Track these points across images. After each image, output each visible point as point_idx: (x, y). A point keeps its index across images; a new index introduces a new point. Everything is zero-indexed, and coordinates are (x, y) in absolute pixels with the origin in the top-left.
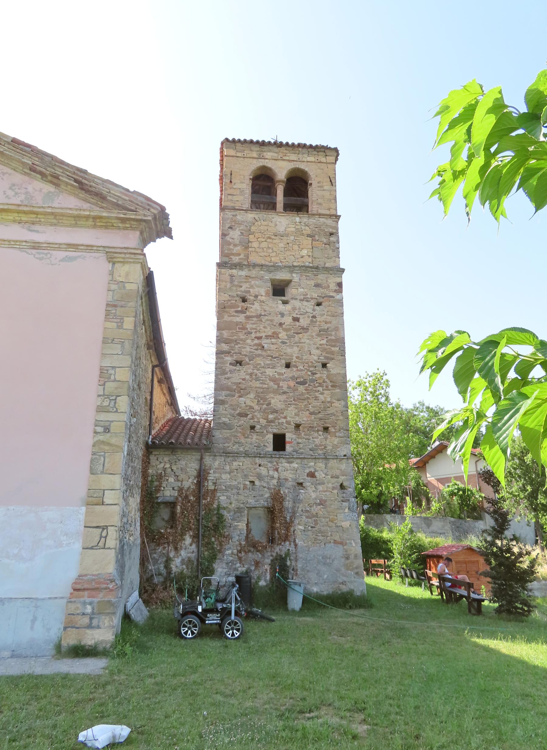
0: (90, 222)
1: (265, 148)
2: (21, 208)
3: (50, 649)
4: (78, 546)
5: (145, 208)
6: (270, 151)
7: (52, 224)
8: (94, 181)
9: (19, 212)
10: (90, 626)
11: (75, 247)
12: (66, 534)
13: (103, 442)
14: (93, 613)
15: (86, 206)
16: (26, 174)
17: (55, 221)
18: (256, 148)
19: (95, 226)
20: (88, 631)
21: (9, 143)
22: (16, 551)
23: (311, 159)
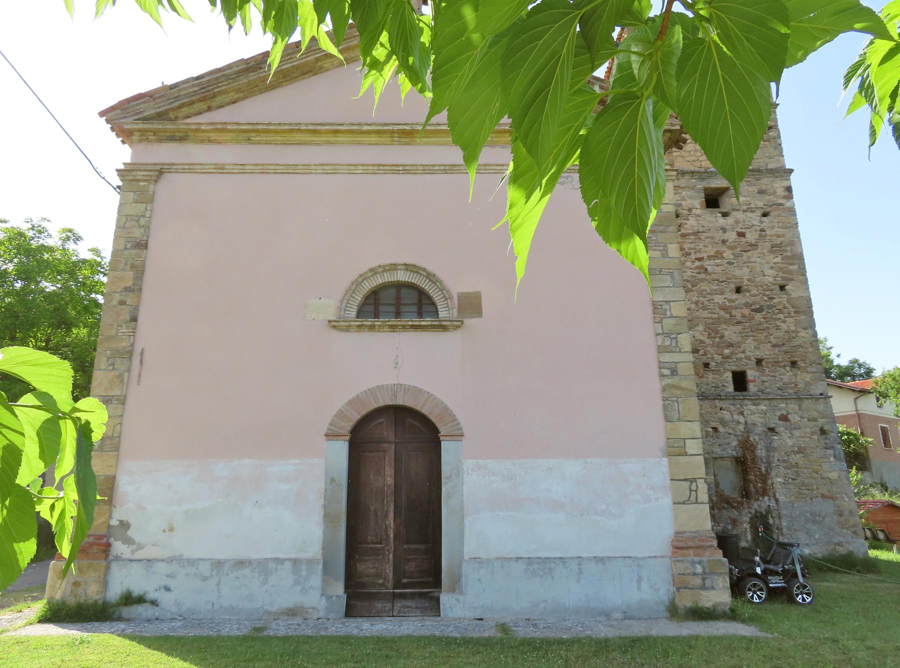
10: (703, 587)
14: (704, 573)
20: (702, 592)
22: (604, 507)
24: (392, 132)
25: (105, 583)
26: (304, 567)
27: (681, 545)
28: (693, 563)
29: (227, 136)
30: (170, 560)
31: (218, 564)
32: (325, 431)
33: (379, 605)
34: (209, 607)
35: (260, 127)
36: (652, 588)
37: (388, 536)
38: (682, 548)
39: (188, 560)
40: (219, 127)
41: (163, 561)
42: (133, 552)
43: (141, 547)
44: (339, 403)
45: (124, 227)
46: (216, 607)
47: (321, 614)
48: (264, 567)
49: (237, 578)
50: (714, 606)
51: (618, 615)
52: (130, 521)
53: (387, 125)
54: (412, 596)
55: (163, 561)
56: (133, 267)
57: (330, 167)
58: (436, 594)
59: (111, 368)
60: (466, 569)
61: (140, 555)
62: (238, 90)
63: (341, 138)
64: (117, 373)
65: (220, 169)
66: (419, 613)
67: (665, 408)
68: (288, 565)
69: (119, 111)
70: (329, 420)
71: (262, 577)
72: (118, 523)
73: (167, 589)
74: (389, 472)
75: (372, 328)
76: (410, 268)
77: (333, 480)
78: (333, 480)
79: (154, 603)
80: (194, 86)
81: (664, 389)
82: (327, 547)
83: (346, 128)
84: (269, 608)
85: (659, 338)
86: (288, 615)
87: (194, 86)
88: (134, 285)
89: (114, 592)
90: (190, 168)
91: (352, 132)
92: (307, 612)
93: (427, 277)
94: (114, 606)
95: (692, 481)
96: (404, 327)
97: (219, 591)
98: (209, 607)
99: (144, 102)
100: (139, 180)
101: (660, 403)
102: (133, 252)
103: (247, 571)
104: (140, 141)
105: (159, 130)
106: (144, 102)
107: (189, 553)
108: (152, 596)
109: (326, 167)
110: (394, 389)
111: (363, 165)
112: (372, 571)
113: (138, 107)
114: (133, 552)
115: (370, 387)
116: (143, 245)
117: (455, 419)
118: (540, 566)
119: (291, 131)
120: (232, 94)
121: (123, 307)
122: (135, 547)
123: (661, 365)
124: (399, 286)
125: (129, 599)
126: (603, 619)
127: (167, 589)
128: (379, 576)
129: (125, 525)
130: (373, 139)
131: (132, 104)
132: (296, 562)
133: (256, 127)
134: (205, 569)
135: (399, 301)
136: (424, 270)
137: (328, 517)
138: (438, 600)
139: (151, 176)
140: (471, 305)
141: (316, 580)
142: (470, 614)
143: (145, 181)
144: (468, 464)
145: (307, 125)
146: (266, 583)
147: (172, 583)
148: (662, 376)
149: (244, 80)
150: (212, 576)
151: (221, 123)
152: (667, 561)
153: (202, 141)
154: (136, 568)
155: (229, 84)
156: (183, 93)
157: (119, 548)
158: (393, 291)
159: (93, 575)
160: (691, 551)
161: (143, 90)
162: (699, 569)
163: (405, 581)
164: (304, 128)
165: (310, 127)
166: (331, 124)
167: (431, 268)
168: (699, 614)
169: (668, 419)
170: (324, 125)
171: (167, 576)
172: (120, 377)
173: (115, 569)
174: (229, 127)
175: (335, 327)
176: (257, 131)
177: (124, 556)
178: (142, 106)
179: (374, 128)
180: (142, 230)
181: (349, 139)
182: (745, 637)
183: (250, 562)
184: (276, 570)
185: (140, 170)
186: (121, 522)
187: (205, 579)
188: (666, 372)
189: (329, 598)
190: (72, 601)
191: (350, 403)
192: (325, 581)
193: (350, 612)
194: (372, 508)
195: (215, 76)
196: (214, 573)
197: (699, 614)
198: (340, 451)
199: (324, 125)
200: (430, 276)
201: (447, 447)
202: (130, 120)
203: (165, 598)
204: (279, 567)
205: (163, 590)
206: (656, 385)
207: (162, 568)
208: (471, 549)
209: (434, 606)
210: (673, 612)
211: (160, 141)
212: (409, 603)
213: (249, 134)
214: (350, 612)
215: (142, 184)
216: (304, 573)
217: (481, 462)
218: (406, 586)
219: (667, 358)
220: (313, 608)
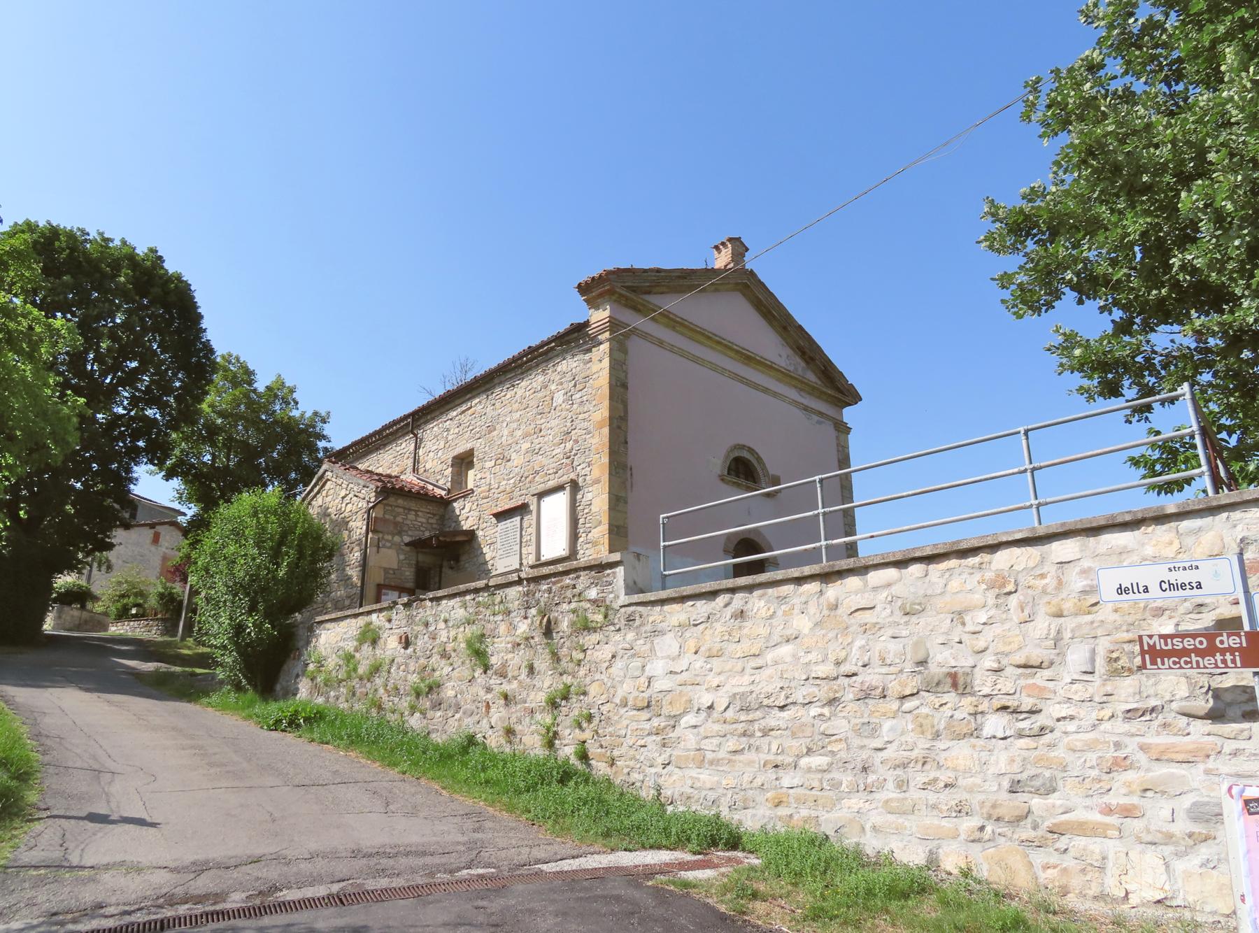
63: (730, 353)
91: (726, 346)
130: (732, 354)
135: (743, 470)
200: (759, 459)
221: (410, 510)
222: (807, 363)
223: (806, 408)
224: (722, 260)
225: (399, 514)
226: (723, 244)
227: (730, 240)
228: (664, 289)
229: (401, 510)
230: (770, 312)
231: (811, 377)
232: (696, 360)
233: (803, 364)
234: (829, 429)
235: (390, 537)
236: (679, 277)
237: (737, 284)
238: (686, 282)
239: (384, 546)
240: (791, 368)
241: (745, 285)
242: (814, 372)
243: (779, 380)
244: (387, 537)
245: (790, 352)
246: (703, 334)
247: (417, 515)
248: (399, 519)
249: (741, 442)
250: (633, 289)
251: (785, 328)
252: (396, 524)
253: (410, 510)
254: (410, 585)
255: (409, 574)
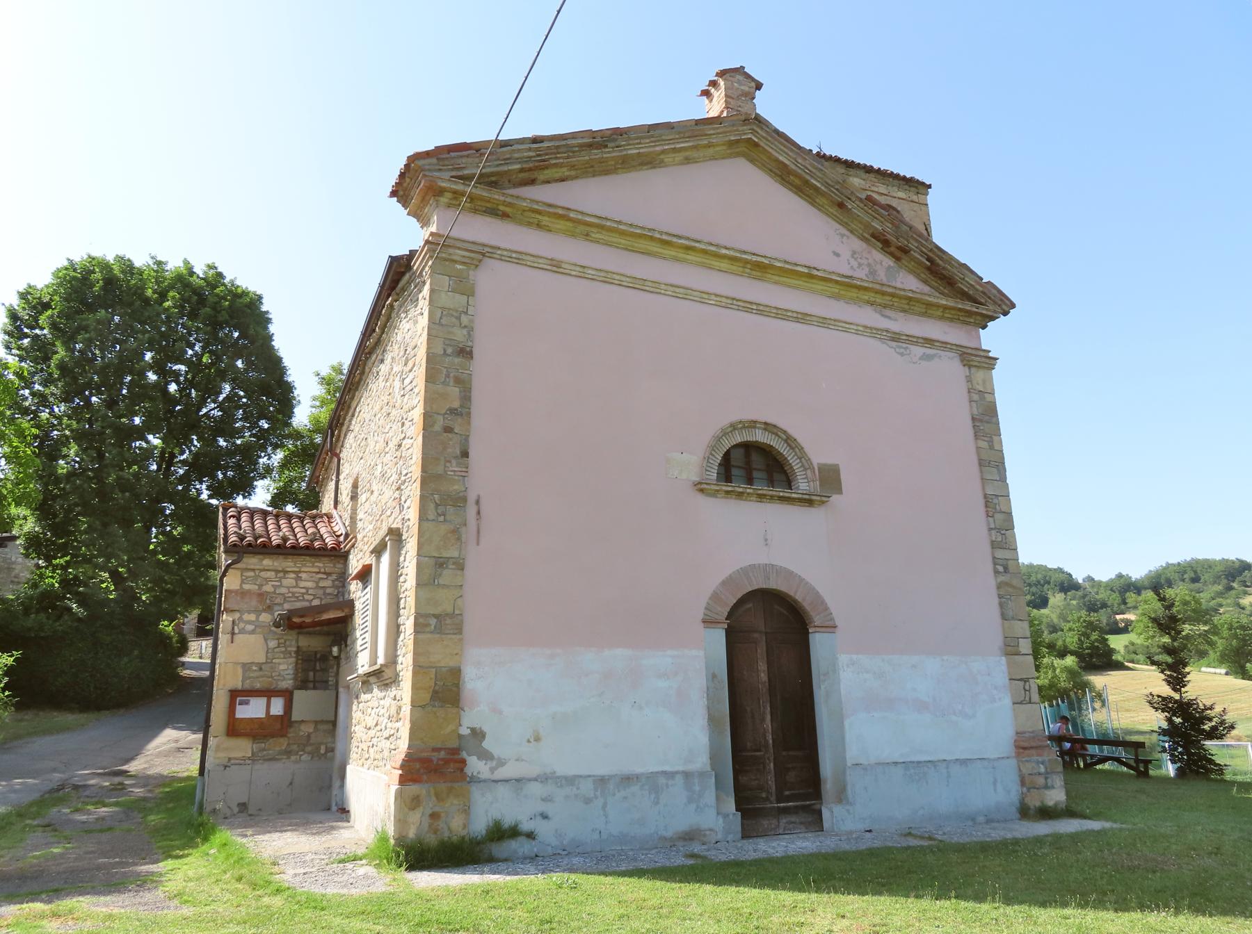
0: (939, 313)
1: (852, 171)
2: (885, 289)
3: (1013, 812)
4: (1007, 701)
5: (995, 303)
6: (857, 176)
7: (904, 311)
8: (950, 264)
9: (877, 292)
10: (1046, 787)
11: (929, 342)
12: (996, 688)
13: (1007, 584)
14: (1047, 773)
15: (927, 289)
16: (863, 239)
17: (907, 307)
18: (841, 169)
19: (942, 318)
20: (1047, 792)
21: (861, 200)
22: (960, 707)
23: (901, 194)
24: (747, 262)
25: (466, 810)
26: (696, 781)
27: (1024, 746)
28: (1038, 762)
29: (561, 225)
30: (544, 779)
31: (602, 781)
32: (701, 616)
33: (765, 823)
34: (596, 836)
35: (608, 224)
36: (995, 790)
37: (767, 742)
38: (1024, 748)
39: (566, 778)
40: (560, 211)
41: (535, 780)
42: (492, 770)
43: (501, 763)
44: (712, 581)
45: (440, 324)
46: (604, 836)
47: (720, 837)
48: (653, 782)
49: (625, 798)
50: (1056, 805)
51: (981, 819)
52: (485, 729)
53: (745, 252)
54: (795, 810)
55: (535, 780)
56: (458, 381)
57: (681, 290)
58: (817, 807)
59: (442, 519)
60: (851, 777)
61: (502, 773)
62: (572, 167)
63: (716, 263)
64: (452, 527)
65: (556, 266)
66: (804, 829)
67: (1001, 605)
68: (679, 780)
69: (434, 161)
70: (704, 605)
71: (653, 796)
72: (469, 731)
73: (545, 816)
74: (762, 666)
75: (740, 495)
76: (768, 427)
77: (714, 676)
78: (714, 676)
79: (530, 836)
80: (530, 150)
81: (999, 587)
82: (714, 757)
83: (703, 246)
84: (665, 834)
85: (993, 532)
86: (685, 840)
87: (530, 150)
88: (461, 406)
89: (479, 825)
90: (517, 258)
91: (705, 252)
92: (705, 835)
93: (786, 441)
94: (479, 843)
95: (1025, 680)
96: (772, 497)
97: (606, 816)
98: (596, 836)
99: (468, 156)
100: (456, 262)
101: (996, 601)
102: (457, 360)
103: (635, 788)
104: (449, 206)
105: (481, 198)
106: (468, 156)
107: (563, 769)
108: (526, 826)
109: (677, 290)
110: (767, 569)
111: (717, 295)
112: (755, 783)
113: (459, 161)
114: (492, 770)
115: (743, 565)
116: (465, 353)
117: (827, 609)
118: (915, 769)
119: (640, 236)
120: (565, 169)
121: (450, 435)
122: (494, 763)
123: (995, 561)
124: (748, 447)
125: (501, 832)
126: (970, 823)
127: (545, 816)
128: (761, 788)
129: (478, 734)
130: (724, 265)
131: (452, 154)
132: (687, 775)
133: (604, 223)
134: (587, 788)
135: (755, 464)
136: (785, 432)
137: (712, 720)
138: (820, 813)
139: (473, 259)
140: (830, 479)
141: (710, 796)
142: (862, 826)
143: (463, 263)
144: (843, 659)
145: (661, 233)
146: (657, 803)
147: (547, 808)
148: (996, 572)
149: (585, 157)
150: (596, 797)
151: (563, 208)
152: (1013, 762)
153: (529, 224)
154: (503, 791)
155: (568, 157)
156: (516, 155)
157: (475, 765)
158: (742, 451)
159: (455, 802)
160: (1033, 751)
161: (469, 139)
162: (1042, 769)
163: (787, 793)
164: (658, 236)
165: (664, 237)
166: (688, 239)
167: (791, 432)
168: (1046, 813)
169: (1004, 617)
170: (680, 237)
171: (543, 800)
172: (455, 531)
173: (476, 793)
174: (572, 215)
175: (702, 490)
176: (602, 227)
177: (482, 776)
178: (464, 160)
179: (731, 253)
180: (465, 332)
181: (699, 259)
182: (1093, 831)
183: (638, 777)
184: (667, 786)
185: (459, 248)
186: (473, 730)
187: (588, 801)
188: (1001, 569)
189: (726, 816)
190: (432, 840)
191: (724, 583)
192: (718, 798)
193: (746, 835)
194: (748, 709)
195: (557, 144)
196: (598, 793)
197: (1046, 813)
198: (718, 638)
199: (680, 237)
200: (789, 440)
201: (819, 643)
202: (446, 175)
203: (544, 830)
204: (670, 782)
205: (539, 818)
206: (992, 582)
207: (536, 789)
208: (853, 753)
209: (815, 821)
210: (1025, 812)
211: (475, 211)
212: (793, 818)
213: (588, 229)
214: (746, 835)
215: (459, 267)
216: (697, 788)
217: (854, 657)
218: (788, 799)
219: (1000, 554)
220: (711, 830)
221: (286, 572)
222: (898, 259)
223: (896, 337)
224: (715, 107)
225: (267, 580)
226: (713, 84)
227: (722, 74)
228: (565, 172)
229: (271, 574)
230: (806, 182)
231: (909, 282)
232: (638, 285)
233: (888, 262)
234: (950, 366)
235: (252, 617)
236: (590, 146)
237: (731, 144)
238: (609, 154)
239: (242, 631)
240: (861, 274)
241: (741, 133)
242: (911, 272)
243: (836, 297)
244: (246, 617)
245: (857, 244)
246: (652, 238)
247: (298, 579)
248: (268, 588)
249: (748, 416)
250: (491, 181)
251: (841, 205)
252: (261, 596)
253: (286, 572)
254: (287, 684)
255: (285, 669)
